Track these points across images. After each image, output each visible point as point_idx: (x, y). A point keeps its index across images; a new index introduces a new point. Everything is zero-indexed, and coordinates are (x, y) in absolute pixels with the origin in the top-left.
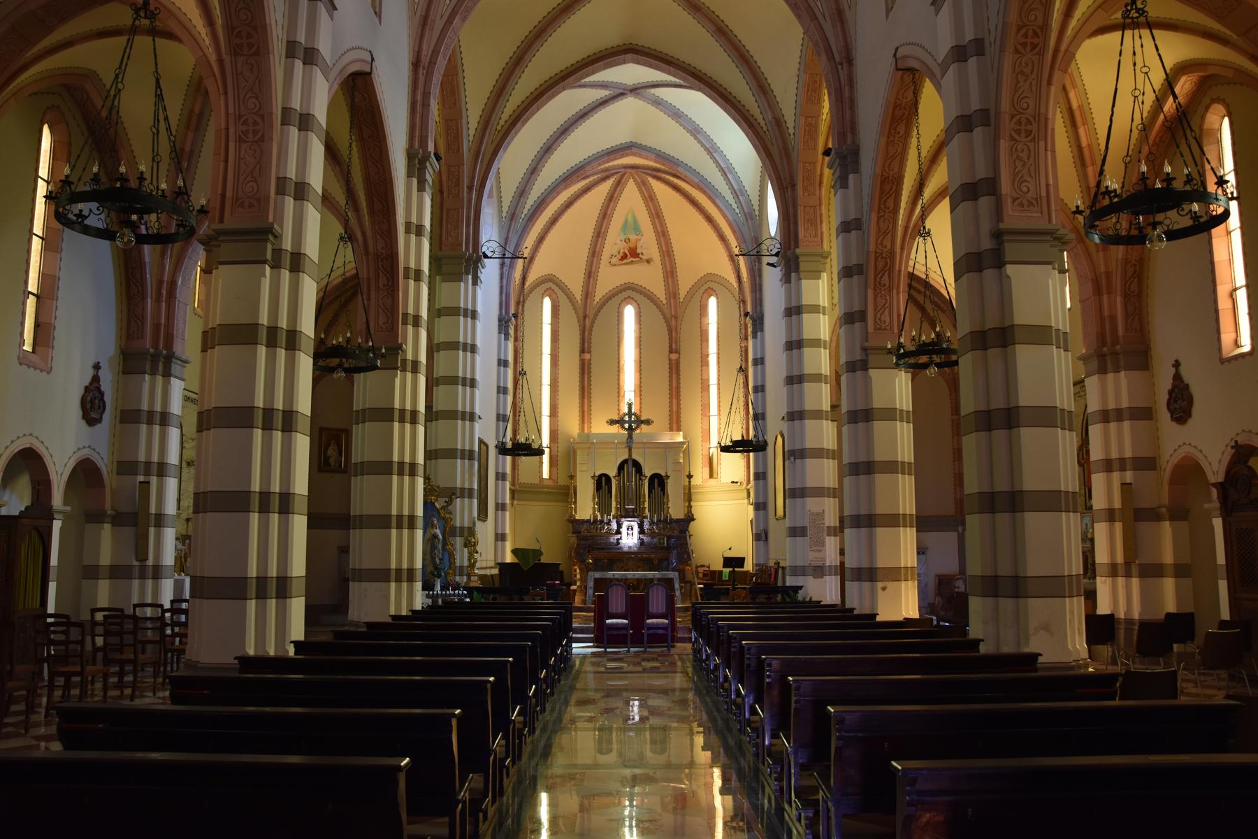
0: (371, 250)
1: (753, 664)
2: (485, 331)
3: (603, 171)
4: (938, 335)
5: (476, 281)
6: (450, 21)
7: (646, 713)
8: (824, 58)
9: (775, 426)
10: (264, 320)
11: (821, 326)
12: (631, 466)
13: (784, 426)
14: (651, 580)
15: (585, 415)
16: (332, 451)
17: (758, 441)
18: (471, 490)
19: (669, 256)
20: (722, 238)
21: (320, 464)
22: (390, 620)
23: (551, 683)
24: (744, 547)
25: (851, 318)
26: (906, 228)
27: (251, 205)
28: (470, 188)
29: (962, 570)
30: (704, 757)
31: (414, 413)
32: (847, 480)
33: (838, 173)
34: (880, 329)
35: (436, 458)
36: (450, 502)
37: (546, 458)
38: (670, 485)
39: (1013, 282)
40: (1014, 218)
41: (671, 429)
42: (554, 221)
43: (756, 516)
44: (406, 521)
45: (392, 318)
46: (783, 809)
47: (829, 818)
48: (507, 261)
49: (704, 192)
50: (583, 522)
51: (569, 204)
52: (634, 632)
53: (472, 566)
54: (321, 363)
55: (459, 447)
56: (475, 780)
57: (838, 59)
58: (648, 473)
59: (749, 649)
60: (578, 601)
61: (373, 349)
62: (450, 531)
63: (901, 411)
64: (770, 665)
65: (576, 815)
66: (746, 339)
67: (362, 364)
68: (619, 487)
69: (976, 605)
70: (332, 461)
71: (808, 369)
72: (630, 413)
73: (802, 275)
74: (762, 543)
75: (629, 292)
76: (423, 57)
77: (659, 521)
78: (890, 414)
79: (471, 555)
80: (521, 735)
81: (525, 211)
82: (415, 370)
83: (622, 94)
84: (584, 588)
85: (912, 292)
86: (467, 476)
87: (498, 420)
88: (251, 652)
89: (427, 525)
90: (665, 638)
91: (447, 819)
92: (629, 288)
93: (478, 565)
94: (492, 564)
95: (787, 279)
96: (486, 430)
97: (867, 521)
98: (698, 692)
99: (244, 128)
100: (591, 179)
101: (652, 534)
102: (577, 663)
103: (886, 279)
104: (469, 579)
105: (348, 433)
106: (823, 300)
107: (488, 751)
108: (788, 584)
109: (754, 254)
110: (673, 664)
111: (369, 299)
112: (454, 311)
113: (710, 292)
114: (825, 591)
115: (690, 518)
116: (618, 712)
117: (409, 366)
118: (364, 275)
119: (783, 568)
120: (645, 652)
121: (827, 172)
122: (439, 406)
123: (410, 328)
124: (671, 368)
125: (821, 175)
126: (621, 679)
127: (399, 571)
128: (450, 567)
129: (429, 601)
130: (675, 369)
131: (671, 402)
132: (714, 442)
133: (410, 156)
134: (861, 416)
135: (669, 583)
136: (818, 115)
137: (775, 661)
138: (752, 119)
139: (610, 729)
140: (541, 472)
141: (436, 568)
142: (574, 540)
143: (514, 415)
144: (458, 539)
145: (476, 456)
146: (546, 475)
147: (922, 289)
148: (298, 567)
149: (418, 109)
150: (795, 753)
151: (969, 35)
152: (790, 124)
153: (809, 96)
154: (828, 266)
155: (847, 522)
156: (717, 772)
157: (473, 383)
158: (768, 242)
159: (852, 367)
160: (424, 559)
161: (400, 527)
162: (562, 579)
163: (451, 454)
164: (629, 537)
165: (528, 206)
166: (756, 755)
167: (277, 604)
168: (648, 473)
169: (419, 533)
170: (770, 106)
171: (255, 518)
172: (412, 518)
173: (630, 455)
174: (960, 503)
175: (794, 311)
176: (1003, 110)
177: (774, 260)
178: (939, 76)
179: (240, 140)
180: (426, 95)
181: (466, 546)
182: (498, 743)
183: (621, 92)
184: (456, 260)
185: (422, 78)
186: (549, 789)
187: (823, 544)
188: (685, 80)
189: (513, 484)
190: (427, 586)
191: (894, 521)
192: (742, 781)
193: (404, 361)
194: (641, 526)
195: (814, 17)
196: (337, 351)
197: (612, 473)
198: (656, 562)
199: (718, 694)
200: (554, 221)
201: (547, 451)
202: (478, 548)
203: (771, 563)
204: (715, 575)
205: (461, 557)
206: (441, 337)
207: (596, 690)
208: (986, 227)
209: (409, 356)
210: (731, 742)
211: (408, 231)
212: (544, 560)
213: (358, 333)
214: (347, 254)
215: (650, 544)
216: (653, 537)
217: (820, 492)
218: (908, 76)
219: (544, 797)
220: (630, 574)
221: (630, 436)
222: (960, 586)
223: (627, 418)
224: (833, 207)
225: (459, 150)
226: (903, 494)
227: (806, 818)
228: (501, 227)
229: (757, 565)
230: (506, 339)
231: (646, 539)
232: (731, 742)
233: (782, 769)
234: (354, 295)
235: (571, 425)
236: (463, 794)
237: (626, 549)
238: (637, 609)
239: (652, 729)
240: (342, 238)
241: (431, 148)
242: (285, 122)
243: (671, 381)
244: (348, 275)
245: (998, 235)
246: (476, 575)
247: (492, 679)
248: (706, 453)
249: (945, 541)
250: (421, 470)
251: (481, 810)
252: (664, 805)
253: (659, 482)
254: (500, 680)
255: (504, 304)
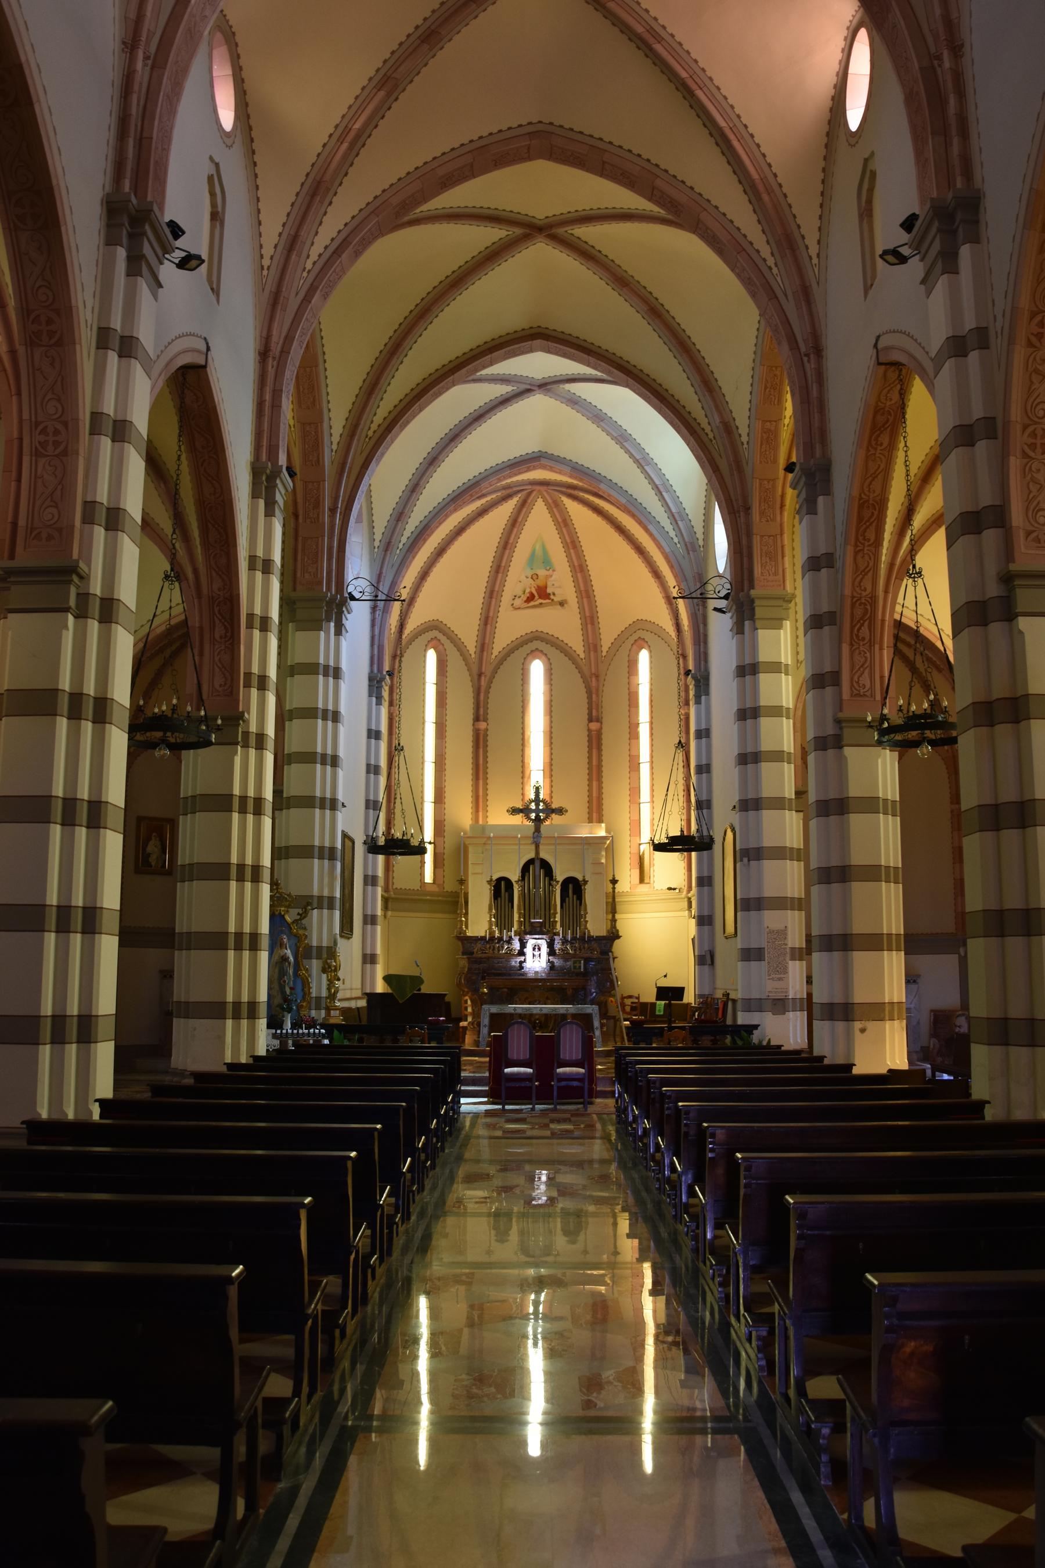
0: (205, 590)
1: (692, 1132)
2: (351, 695)
3: (505, 488)
4: (932, 704)
5: (339, 630)
6: (307, 299)
7: (555, 1194)
8: (785, 346)
9: (724, 817)
10: (65, 683)
11: (783, 690)
12: (538, 868)
13: (735, 818)
14: (564, 1017)
15: (479, 802)
16: (153, 847)
17: (701, 837)
18: (331, 899)
19: (588, 597)
20: (657, 574)
21: (137, 863)
22: (224, 1069)
23: (432, 1152)
24: (684, 974)
25: (820, 680)
26: (891, 565)
27: (50, 537)
28: (333, 510)
29: (965, 1006)
30: (629, 1248)
31: (259, 801)
32: (815, 889)
33: (803, 495)
34: (859, 695)
35: (287, 858)
36: (304, 915)
37: (429, 857)
38: (590, 895)
39: (1028, 638)
40: (1028, 557)
41: (590, 820)
42: (440, 551)
43: (700, 932)
44: (246, 941)
45: (231, 678)
46: (729, 1325)
47: (787, 1338)
48: (381, 604)
49: (633, 516)
50: (476, 939)
51: (459, 531)
52: (540, 1085)
53: (332, 997)
54: (139, 737)
55: (317, 843)
56: (331, 1283)
57: (803, 349)
58: (560, 876)
59: (687, 1113)
60: (468, 1043)
61: (205, 719)
62: (304, 952)
63: (885, 800)
64: (713, 1135)
65: (460, 1331)
66: (687, 703)
67: (193, 739)
68: (523, 895)
69: (980, 1055)
70: (153, 860)
71: (766, 745)
72: (537, 800)
73: (758, 624)
74: (706, 968)
75: (535, 643)
76: (273, 345)
77: (574, 938)
78: (871, 805)
79: (331, 984)
80: (391, 1223)
81: (404, 540)
82: (260, 746)
83: (528, 391)
84: (477, 1025)
85: (900, 645)
86: (326, 880)
87: (367, 807)
88: (44, 1115)
89: (275, 943)
90: (580, 1092)
91: (292, 1337)
92: (537, 638)
93: (340, 995)
94: (358, 993)
95: (739, 629)
96: (351, 821)
97: (840, 943)
98: (622, 1165)
99: (42, 438)
100: (488, 498)
101: (565, 956)
102: (468, 1124)
103: (865, 631)
104: (328, 1014)
105: (173, 823)
106: (786, 655)
107: (348, 1248)
108: (740, 1022)
109: (697, 597)
110: (591, 1126)
111: (201, 654)
112: (311, 669)
113: (640, 643)
114: (787, 1031)
115: (614, 935)
116: (517, 1191)
117: (253, 741)
118: (195, 622)
119: (734, 1001)
120: (555, 1110)
121: (790, 493)
122: (291, 789)
123: (254, 692)
124: (590, 741)
125: (783, 496)
126: (522, 1145)
127: (237, 1005)
128: (304, 999)
129: (277, 1042)
130: (595, 742)
131: (590, 785)
132: (646, 836)
133: (256, 471)
134: (833, 807)
135: (585, 1020)
136: (780, 418)
137: (719, 1130)
138: (694, 425)
139: (509, 1215)
140: (422, 874)
141: (286, 1000)
142: (464, 963)
143: (389, 801)
144: (315, 962)
145: (338, 855)
146: (428, 878)
147: (912, 642)
148: (106, 1003)
149: (266, 411)
150: (745, 1253)
151: (970, 322)
152: (743, 430)
153: (767, 396)
154: (791, 612)
155: (815, 943)
156: (647, 1268)
157: (335, 761)
158: (714, 582)
159: (822, 743)
160: (270, 988)
161: (239, 948)
162: (448, 1014)
163: (306, 852)
164: (536, 960)
165: (407, 533)
166: (696, 1250)
167: (78, 1050)
168: (560, 876)
169: (264, 956)
170: (717, 407)
171: (51, 939)
172: (255, 937)
173: (537, 852)
174: (961, 916)
175: (748, 670)
176: (1013, 418)
177: (722, 604)
178: (931, 374)
179: (37, 454)
180: (277, 393)
181: (324, 970)
182: (361, 1236)
183: (527, 388)
184: (314, 601)
185: (271, 371)
186: (428, 1293)
187: (785, 971)
188: (608, 373)
189: (386, 889)
190: (274, 1023)
191: (876, 942)
192: (678, 1284)
193: (246, 734)
194: (551, 945)
195: (773, 296)
196: (160, 722)
197: (514, 876)
198: (570, 992)
199: (647, 1168)
200: (440, 552)
201: (430, 848)
202: (340, 974)
203: (719, 994)
204: (646, 1008)
205: (319, 986)
206: (294, 702)
207: (491, 1162)
208: (992, 569)
209: (253, 728)
210: (664, 1235)
211: (252, 567)
212: (426, 989)
213: (187, 697)
214: (174, 595)
215: (562, 968)
216: (566, 960)
217: (782, 903)
218: (893, 373)
219: (423, 1303)
220: (536, 1008)
221: (537, 830)
222: (962, 1025)
223: (533, 806)
224: (797, 537)
225: (318, 462)
226: (887, 908)
227: (759, 1338)
228: (372, 560)
229: (700, 996)
230: (379, 703)
231: (557, 962)
232: (664, 1235)
233: (728, 1272)
234: (182, 647)
235: (462, 815)
236: (315, 1306)
237: (531, 975)
238: (545, 1054)
239: (565, 1213)
240: (167, 577)
241: (283, 460)
242: (95, 430)
243: (590, 758)
244: (173, 622)
245: (1007, 579)
246: (336, 1009)
247: (353, 1154)
248: (634, 850)
249: (941, 967)
250: (266, 875)
251: (338, 1326)
252: (575, 1319)
253: (574, 888)
254: (365, 1156)
255: (375, 659)
